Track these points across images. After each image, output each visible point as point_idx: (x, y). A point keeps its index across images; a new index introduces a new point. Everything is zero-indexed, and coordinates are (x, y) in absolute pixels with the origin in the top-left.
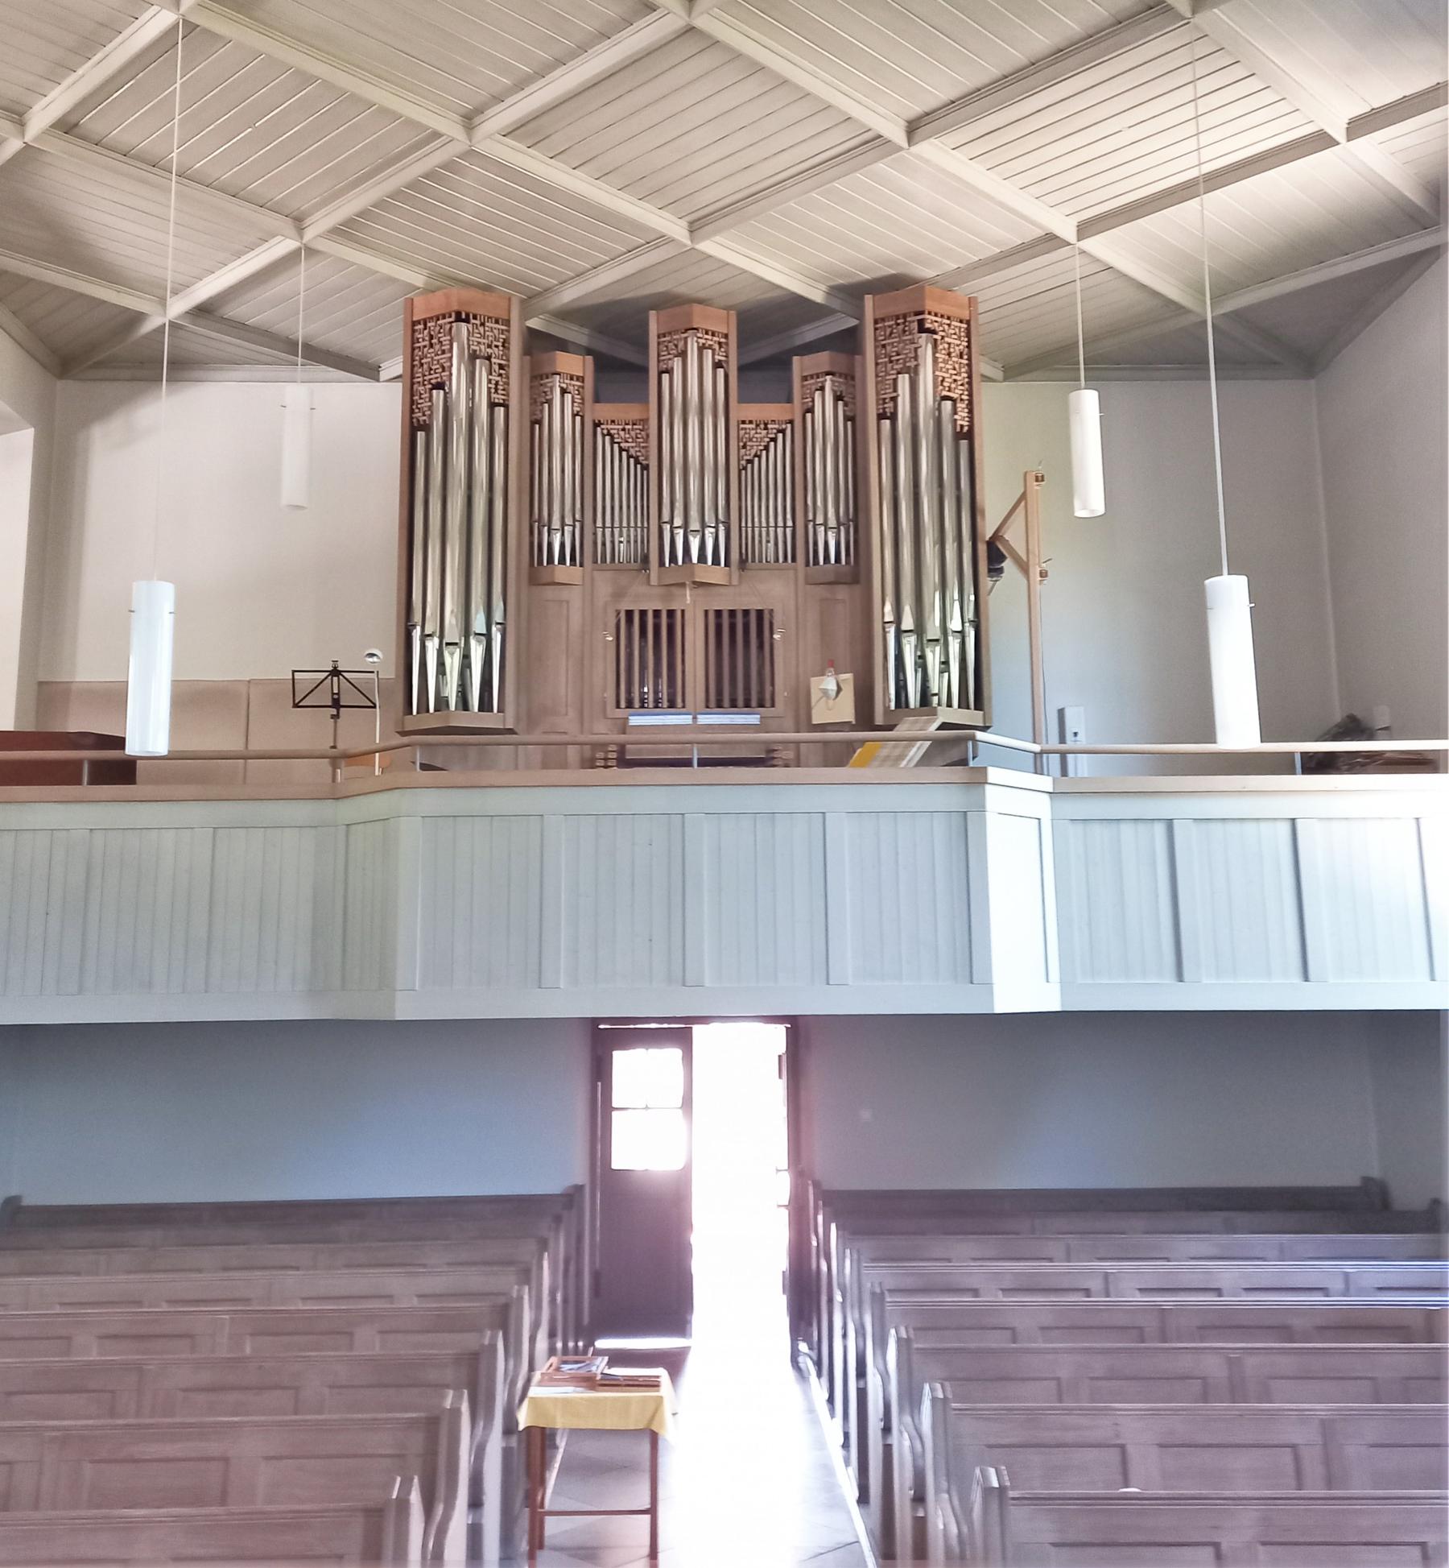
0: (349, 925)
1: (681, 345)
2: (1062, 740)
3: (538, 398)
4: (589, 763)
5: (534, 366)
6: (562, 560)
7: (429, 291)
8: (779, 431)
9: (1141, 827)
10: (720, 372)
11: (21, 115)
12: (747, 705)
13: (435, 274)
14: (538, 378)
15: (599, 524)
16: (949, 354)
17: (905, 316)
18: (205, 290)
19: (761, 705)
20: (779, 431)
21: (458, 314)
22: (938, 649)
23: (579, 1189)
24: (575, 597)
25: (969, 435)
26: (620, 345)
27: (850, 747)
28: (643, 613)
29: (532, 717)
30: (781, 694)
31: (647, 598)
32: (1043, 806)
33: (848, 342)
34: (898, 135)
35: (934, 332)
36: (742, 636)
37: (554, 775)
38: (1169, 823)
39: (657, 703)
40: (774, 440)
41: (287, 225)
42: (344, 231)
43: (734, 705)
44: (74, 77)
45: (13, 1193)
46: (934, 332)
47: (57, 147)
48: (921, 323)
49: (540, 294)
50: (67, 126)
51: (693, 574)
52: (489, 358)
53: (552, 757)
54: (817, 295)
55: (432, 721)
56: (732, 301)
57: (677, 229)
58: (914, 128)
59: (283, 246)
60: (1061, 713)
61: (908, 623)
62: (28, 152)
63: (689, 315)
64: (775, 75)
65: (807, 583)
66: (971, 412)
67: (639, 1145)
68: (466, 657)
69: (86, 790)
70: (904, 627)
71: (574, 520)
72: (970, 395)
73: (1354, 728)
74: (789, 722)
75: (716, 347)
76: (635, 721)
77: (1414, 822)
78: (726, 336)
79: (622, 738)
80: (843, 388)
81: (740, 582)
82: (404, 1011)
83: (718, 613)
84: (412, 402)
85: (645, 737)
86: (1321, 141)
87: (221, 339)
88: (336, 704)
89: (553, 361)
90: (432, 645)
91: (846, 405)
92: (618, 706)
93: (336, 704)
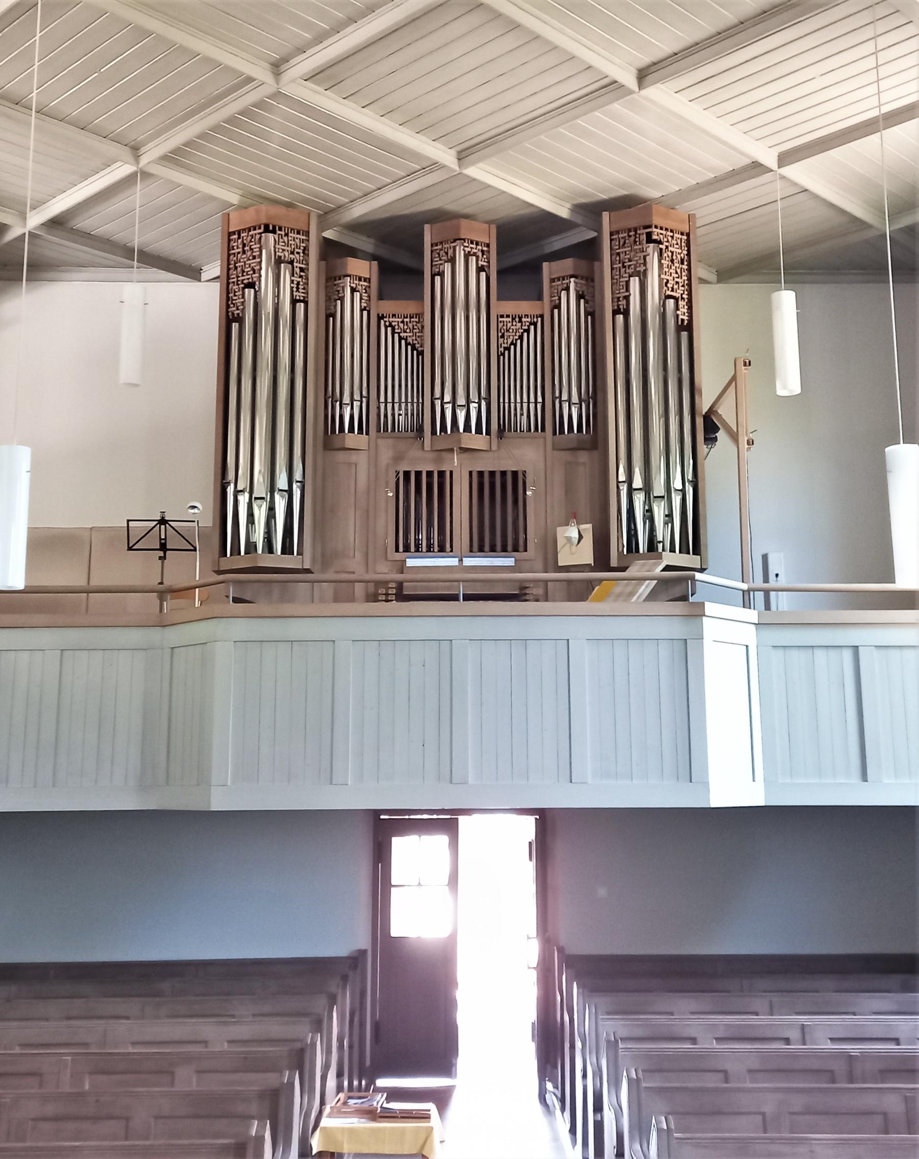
0: (173, 732)
1: (450, 252)
4: (373, 598)
7: (242, 207)
8: (531, 324)
9: (833, 653)
12: (504, 549)
15: (382, 399)
19: (516, 549)
23: (363, 953)
24: (362, 460)
26: (400, 252)
27: (590, 585)
29: (326, 559)
31: (421, 461)
32: (750, 635)
33: (588, 251)
35: (660, 242)
36: (500, 493)
39: (429, 548)
40: (528, 331)
41: (126, 153)
42: (172, 158)
43: (493, 549)
46: (660, 242)
48: (649, 235)
51: (459, 441)
53: (343, 593)
54: (563, 212)
55: (243, 561)
57: (447, 157)
58: (643, 75)
59: (123, 170)
60: (765, 558)
61: (638, 483)
63: (458, 228)
68: (271, 509)
74: (539, 564)
76: (410, 563)
78: (488, 245)
79: (400, 577)
80: (584, 288)
81: (499, 447)
83: (481, 473)
84: (228, 299)
88: (163, 547)
89: (345, 266)
90: (243, 499)
91: (586, 302)
92: (397, 550)
93: (163, 547)
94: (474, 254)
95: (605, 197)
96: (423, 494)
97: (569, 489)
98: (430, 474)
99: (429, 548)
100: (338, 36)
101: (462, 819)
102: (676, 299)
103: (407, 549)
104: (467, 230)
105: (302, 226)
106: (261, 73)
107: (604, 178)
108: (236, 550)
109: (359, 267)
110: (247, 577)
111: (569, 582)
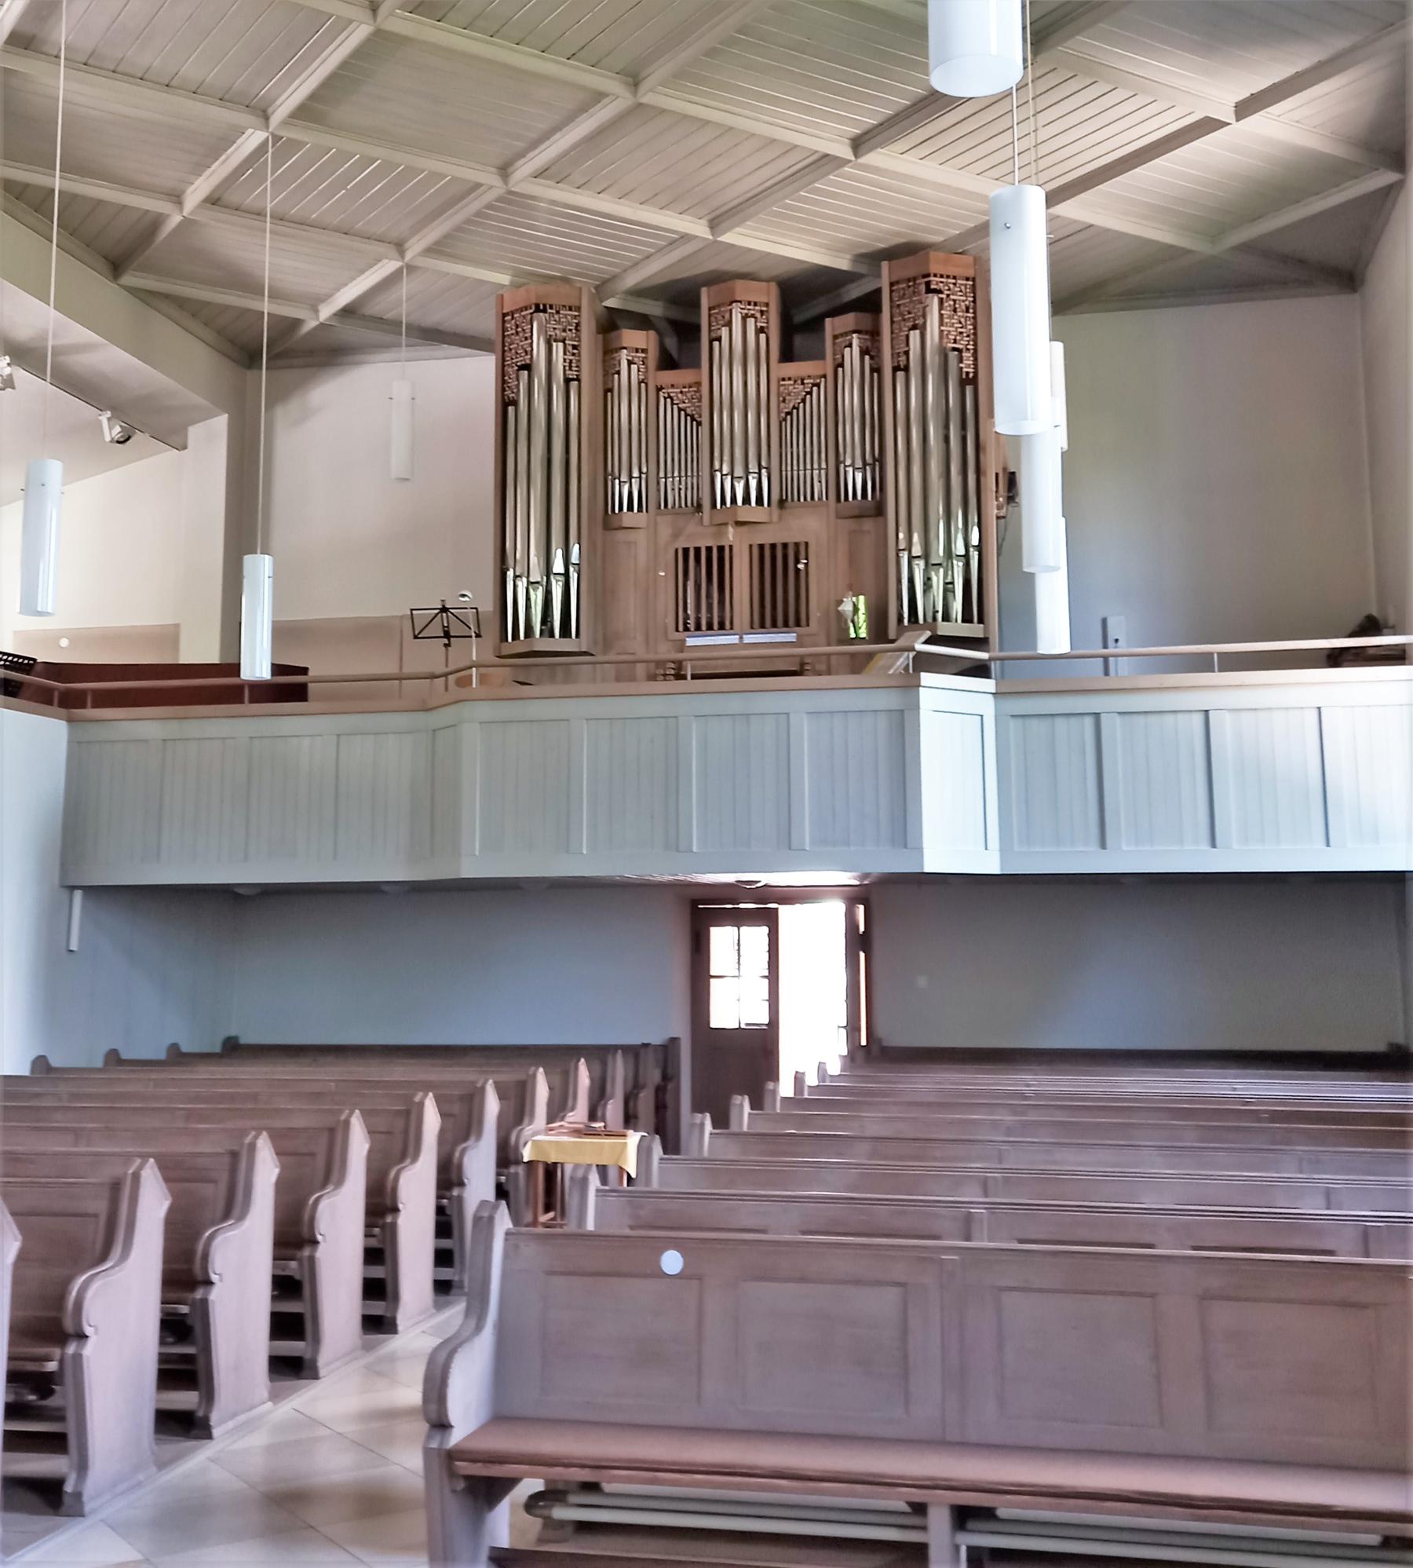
0: (434, 806)
1: (727, 316)
2: (1105, 646)
3: (609, 370)
4: (652, 677)
6: (630, 508)
7: (515, 286)
8: (814, 385)
9: (1073, 720)
10: (763, 336)
11: (178, 196)
12: (786, 624)
13: (517, 273)
14: (609, 352)
15: (662, 474)
16: (955, 310)
17: (915, 279)
18: (346, 296)
19: (798, 624)
20: (814, 385)
21: (537, 306)
22: (941, 570)
23: (674, 1040)
24: (641, 538)
26: (678, 320)
27: (870, 656)
28: (698, 550)
29: (607, 641)
30: (815, 613)
32: (987, 706)
33: (870, 304)
34: (846, 152)
35: (940, 292)
36: (780, 567)
37: (624, 687)
38: (1097, 715)
39: (710, 627)
40: (810, 393)
41: (393, 252)
42: (436, 250)
43: (774, 625)
44: (208, 172)
45: (233, 1033)
46: (940, 292)
47: (207, 217)
48: (928, 284)
49: (609, 280)
50: (213, 201)
51: (735, 514)
52: (563, 341)
53: (625, 672)
54: (843, 264)
56: (774, 273)
57: (699, 229)
58: (858, 144)
59: (389, 266)
60: (1104, 622)
61: (917, 550)
62: (187, 223)
63: (732, 291)
64: (718, 125)
65: (838, 517)
66: (976, 360)
69: (248, 707)
70: (914, 554)
71: (641, 472)
72: (975, 345)
73: (1371, 626)
74: (822, 638)
75: (758, 315)
76: (691, 642)
77: (1316, 712)
78: (767, 305)
79: (680, 656)
80: (869, 344)
81: (780, 518)
82: (469, 870)
83: (761, 547)
84: (504, 382)
85: (715, 654)
86: (1208, 126)
88: (447, 635)
89: (619, 337)
90: (522, 584)
91: (872, 358)
92: (677, 630)
94: (753, 316)
95: (882, 246)
96: (707, 567)
97: (853, 559)
98: (709, 549)
99: (710, 627)
100: (547, 143)
101: (785, 912)
102: (959, 351)
103: (686, 629)
105: (574, 302)
106: (489, 177)
107: (886, 225)
108: (516, 636)
109: (633, 337)
110: (530, 658)
111: (853, 655)
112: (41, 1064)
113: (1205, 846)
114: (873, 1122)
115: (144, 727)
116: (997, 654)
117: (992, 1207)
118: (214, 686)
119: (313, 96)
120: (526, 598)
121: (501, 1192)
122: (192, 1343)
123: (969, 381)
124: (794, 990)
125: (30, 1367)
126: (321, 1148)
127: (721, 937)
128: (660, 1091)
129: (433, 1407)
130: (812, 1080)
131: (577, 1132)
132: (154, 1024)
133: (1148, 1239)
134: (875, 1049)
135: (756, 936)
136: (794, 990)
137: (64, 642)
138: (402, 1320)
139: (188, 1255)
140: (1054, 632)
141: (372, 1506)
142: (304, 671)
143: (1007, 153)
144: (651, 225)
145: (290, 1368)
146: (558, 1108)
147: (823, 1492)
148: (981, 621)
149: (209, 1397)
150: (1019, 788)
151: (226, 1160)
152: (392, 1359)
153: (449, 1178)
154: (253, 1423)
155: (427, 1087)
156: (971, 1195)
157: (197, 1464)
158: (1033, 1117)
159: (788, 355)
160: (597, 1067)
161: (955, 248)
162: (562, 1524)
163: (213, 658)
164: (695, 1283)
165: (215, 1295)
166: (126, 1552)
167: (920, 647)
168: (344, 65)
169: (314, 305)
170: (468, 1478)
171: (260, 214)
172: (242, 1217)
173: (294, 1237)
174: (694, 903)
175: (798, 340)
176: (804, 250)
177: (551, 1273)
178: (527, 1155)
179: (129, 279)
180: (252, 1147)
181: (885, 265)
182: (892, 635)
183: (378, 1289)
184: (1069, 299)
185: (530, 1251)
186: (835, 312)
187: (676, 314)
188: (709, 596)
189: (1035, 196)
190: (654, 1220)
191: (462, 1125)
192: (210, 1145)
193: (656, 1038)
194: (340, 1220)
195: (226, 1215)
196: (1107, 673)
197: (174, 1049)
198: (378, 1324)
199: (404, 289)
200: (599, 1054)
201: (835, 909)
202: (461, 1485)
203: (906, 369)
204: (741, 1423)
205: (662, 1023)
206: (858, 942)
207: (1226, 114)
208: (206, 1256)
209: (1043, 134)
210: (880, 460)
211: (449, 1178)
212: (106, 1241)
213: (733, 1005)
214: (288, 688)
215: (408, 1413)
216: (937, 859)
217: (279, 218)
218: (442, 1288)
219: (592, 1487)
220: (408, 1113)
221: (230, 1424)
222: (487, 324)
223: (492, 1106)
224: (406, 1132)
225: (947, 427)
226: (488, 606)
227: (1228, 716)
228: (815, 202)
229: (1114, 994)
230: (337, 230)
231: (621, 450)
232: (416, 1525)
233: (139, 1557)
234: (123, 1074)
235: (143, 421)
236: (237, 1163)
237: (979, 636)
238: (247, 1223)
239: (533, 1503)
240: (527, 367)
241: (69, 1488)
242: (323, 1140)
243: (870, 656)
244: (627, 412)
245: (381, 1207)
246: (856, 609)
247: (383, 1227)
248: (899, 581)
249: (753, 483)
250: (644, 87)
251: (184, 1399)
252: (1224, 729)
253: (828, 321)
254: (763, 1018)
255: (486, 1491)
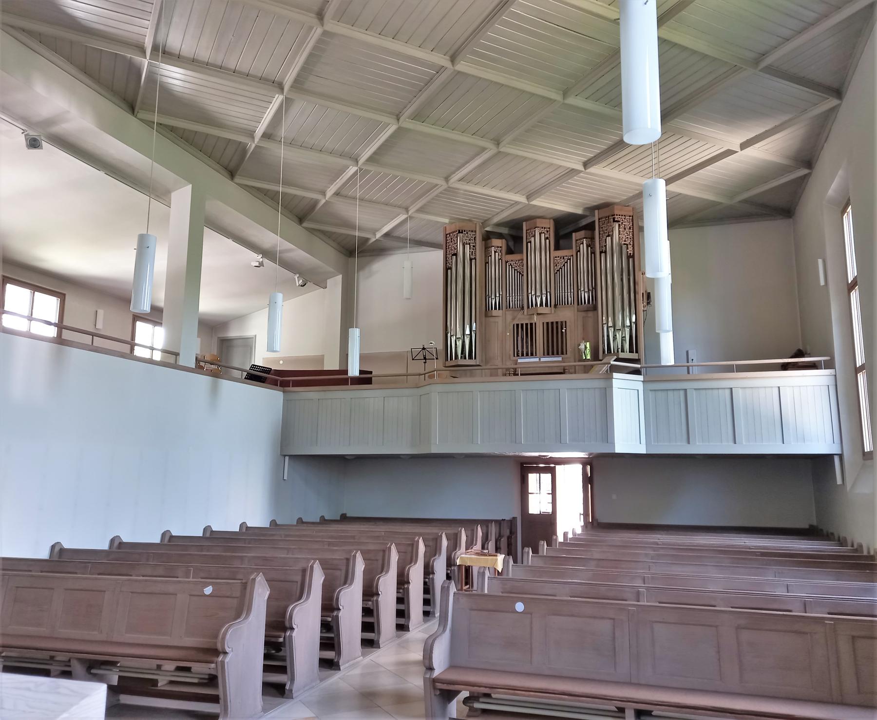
0: (420, 426)
4: (505, 375)
5: (486, 245)
6: (495, 308)
7: (451, 223)
9: (676, 392)
12: (558, 354)
13: (451, 218)
14: (487, 248)
19: (562, 353)
23: (514, 518)
24: (500, 321)
25: (633, 257)
26: (514, 234)
27: (592, 366)
28: (522, 325)
31: (523, 318)
32: (640, 387)
33: (590, 227)
34: (581, 168)
37: (492, 379)
38: (686, 390)
39: (527, 355)
42: (420, 210)
43: (553, 354)
50: (337, 194)
53: (494, 373)
54: (580, 211)
55: (453, 363)
57: (522, 199)
58: (586, 165)
60: (687, 352)
61: (610, 324)
62: (327, 203)
67: (538, 504)
68: (464, 342)
69: (350, 387)
73: (800, 354)
76: (519, 361)
82: (434, 450)
83: (548, 323)
87: (390, 244)
88: (425, 358)
90: (453, 339)
93: (425, 358)
98: (527, 324)
99: (527, 355)
101: (559, 468)
103: (518, 355)
104: (539, 223)
106: (441, 182)
107: (596, 196)
108: (451, 359)
109: (497, 242)
111: (585, 366)
112: (273, 523)
113: (732, 443)
114: (596, 553)
115: (312, 394)
116: (644, 365)
117: (648, 589)
118: (337, 379)
119: (375, 153)
120: (455, 344)
121: (449, 577)
122: (333, 632)
123: (631, 256)
124: (562, 498)
125: (273, 640)
126: (380, 557)
127: (532, 478)
128: (509, 538)
129: (427, 661)
130: (570, 536)
131: (477, 554)
132: (316, 509)
133: (713, 603)
134: (595, 524)
135: (546, 478)
136: (562, 498)
137: (281, 362)
138: (411, 626)
139: (331, 599)
140: (668, 356)
141: (401, 699)
142: (371, 373)
143: (650, 164)
144: (503, 199)
145: (369, 644)
146: (470, 544)
147: (579, 701)
148: (637, 352)
149: (339, 654)
150: (653, 418)
151: (345, 561)
152: (407, 641)
153: (428, 571)
154: (356, 664)
155: (420, 535)
156: (638, 583)
157: (335, 679)
158: (662, 552)
159: (557, 247)
160: (485, 528)
161: (624, 204)
162: (476, 710)
163: (336, 367)
164: (529, 616)
165: (341, 614)
166: (308, 713)
167: (612, 363)
168: (387, 141)
169: (374, 232)
170: (441, 690)
171: (355, 198)
172: (351, 584)
173: (370, 592)
174: (522, 464)
175: (562, 242)
176: (563, 206)
177: (472, 610)
178: (458, 562)
179: (305, 224)
180: (355, 556)
181: (596, 211)
182: (601, 358)
183: (402, 614)
184: (673, 223)
185: (464, 601)
186: (576, 231)
187: (513, 233)
188: (527, 342)
189: (662, 183)
190: (514, 590)
191: (433, 550)
192: (338, 555)
193: (508, 517)
194: (388, 586)
195: (345, 583)
196: (688, 373)
197: (322, 517)
198: (402, 628)
199: (409, 225)
200: (485, 523)
201: (579, 467)
202: (438, 693)
203: (605, 252)
204: (547, 672)
205: (509, 511)
206: (588, 480)
207: (736, 148)
208: (337, 599)
209: (661, 158)
210: (595, 288)
211: (428, 571)
212: (301, 592)
213: (538, 504)
214: (365, 379)
215: (416, 663)
216: (620, 448)
217: (361, 200)
218: (426, 614)
219: (488, 696)
220: (413, 545)
221: (347, 665)
222: (440, 239)
223: (445, 543)
224: (412, 552)
225: (622, 275)
226: (441, 347)
227: (740, 390)
228: (567, 187)
229: (692, 504)
230: (383, 204)
231: (492, 286)
232: (421, 708)
233: (312, 715)
234: (304, 527)
235: (310, 278)
236: (349, 562)
237: (637, 357)
238: (353, 586)
239: (466, 701)
240: (456, 255)
241: (287, 687)
242: (381, 554)
243: (592, 366)
244: (494, 271)
245: (403, 581)
246: (586, 347)
247: (404, 589)
248: (603, 336)
249: (544, 299)
250: (501, 145)
251: (330, 654)
252: (738, 395)
253: (574, 234)
254: (550, 510)
255: (448, 695)
